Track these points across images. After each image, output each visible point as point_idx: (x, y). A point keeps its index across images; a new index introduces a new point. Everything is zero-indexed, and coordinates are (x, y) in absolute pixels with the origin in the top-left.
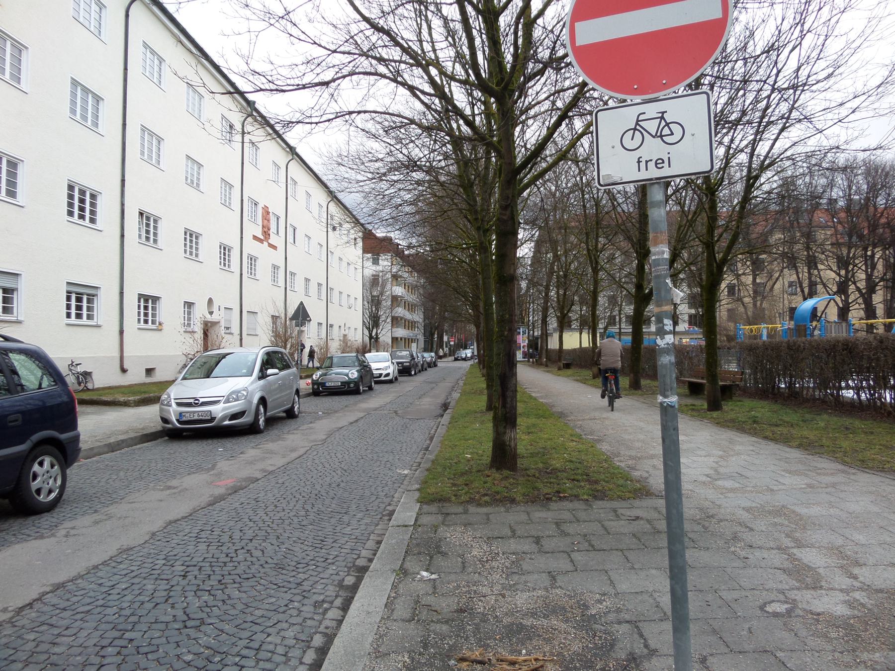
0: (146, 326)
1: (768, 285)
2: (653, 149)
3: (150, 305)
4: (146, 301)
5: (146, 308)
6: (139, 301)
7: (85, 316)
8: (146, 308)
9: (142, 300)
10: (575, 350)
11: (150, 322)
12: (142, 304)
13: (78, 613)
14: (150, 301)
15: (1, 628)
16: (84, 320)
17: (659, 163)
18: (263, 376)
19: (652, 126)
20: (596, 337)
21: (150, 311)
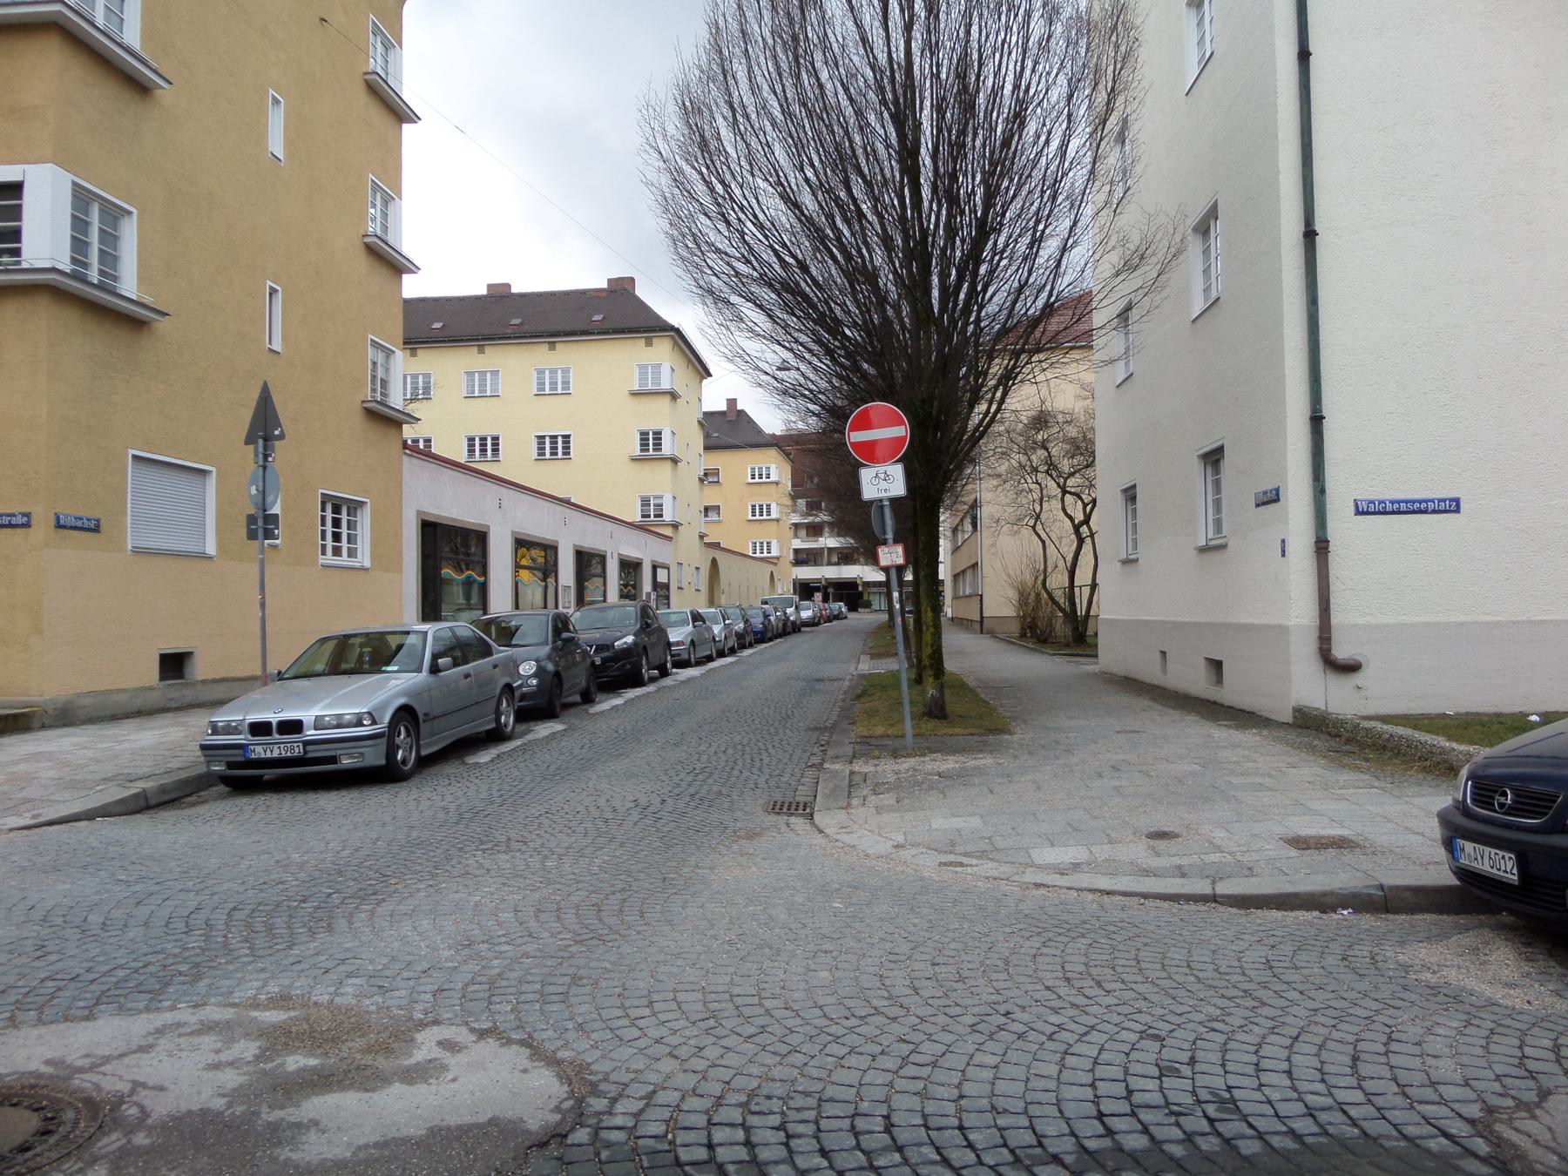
0: (337, 561)
1: (930, 614)
2: (883, 485)
3: (344, 517)
4: (337, 509)
5: (336, 523)
6: (323, 510)
7: (329, 550)
8: (336, 523)
9: (329, 508)
10: (477, 298)
11: (345, 552)
12: (329, 515)
13: (1043, 542)
14: (344, 511)
15: (4, 1165)
16: (344, 560)
17: (886, 490)
18: (435, 669)
19: (882, 476)
20: (841, 252)
21: (344, 530)
